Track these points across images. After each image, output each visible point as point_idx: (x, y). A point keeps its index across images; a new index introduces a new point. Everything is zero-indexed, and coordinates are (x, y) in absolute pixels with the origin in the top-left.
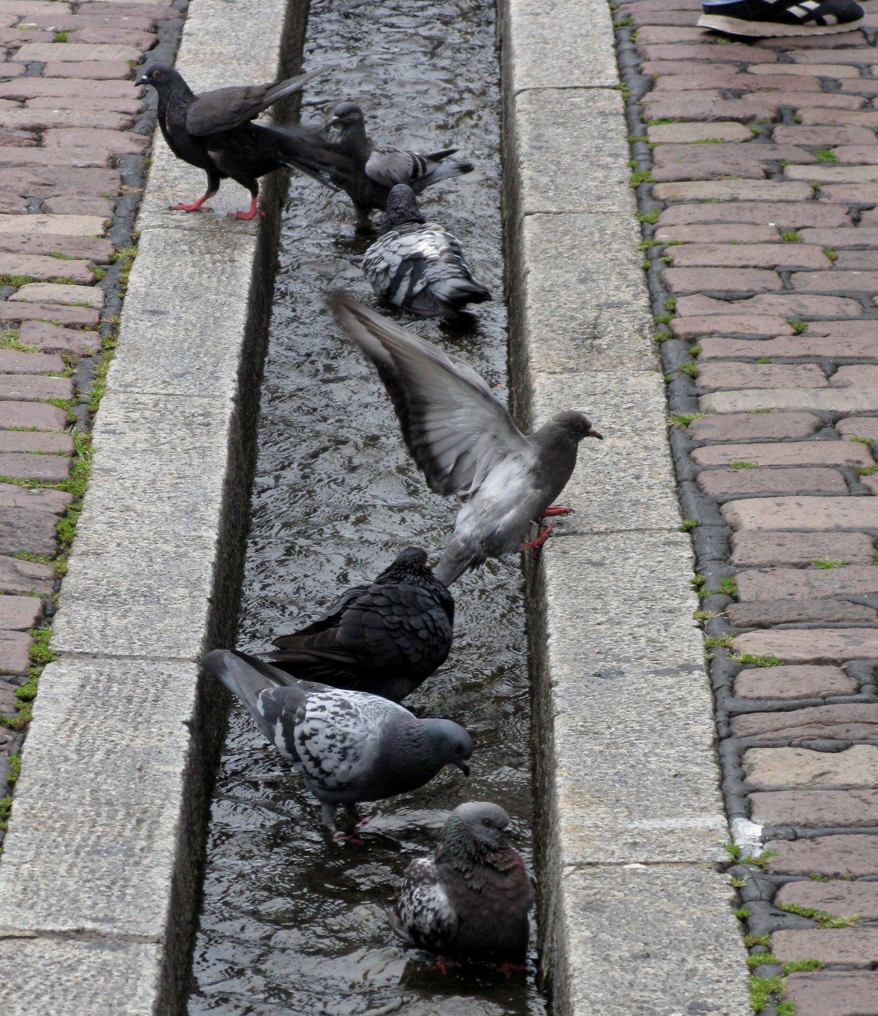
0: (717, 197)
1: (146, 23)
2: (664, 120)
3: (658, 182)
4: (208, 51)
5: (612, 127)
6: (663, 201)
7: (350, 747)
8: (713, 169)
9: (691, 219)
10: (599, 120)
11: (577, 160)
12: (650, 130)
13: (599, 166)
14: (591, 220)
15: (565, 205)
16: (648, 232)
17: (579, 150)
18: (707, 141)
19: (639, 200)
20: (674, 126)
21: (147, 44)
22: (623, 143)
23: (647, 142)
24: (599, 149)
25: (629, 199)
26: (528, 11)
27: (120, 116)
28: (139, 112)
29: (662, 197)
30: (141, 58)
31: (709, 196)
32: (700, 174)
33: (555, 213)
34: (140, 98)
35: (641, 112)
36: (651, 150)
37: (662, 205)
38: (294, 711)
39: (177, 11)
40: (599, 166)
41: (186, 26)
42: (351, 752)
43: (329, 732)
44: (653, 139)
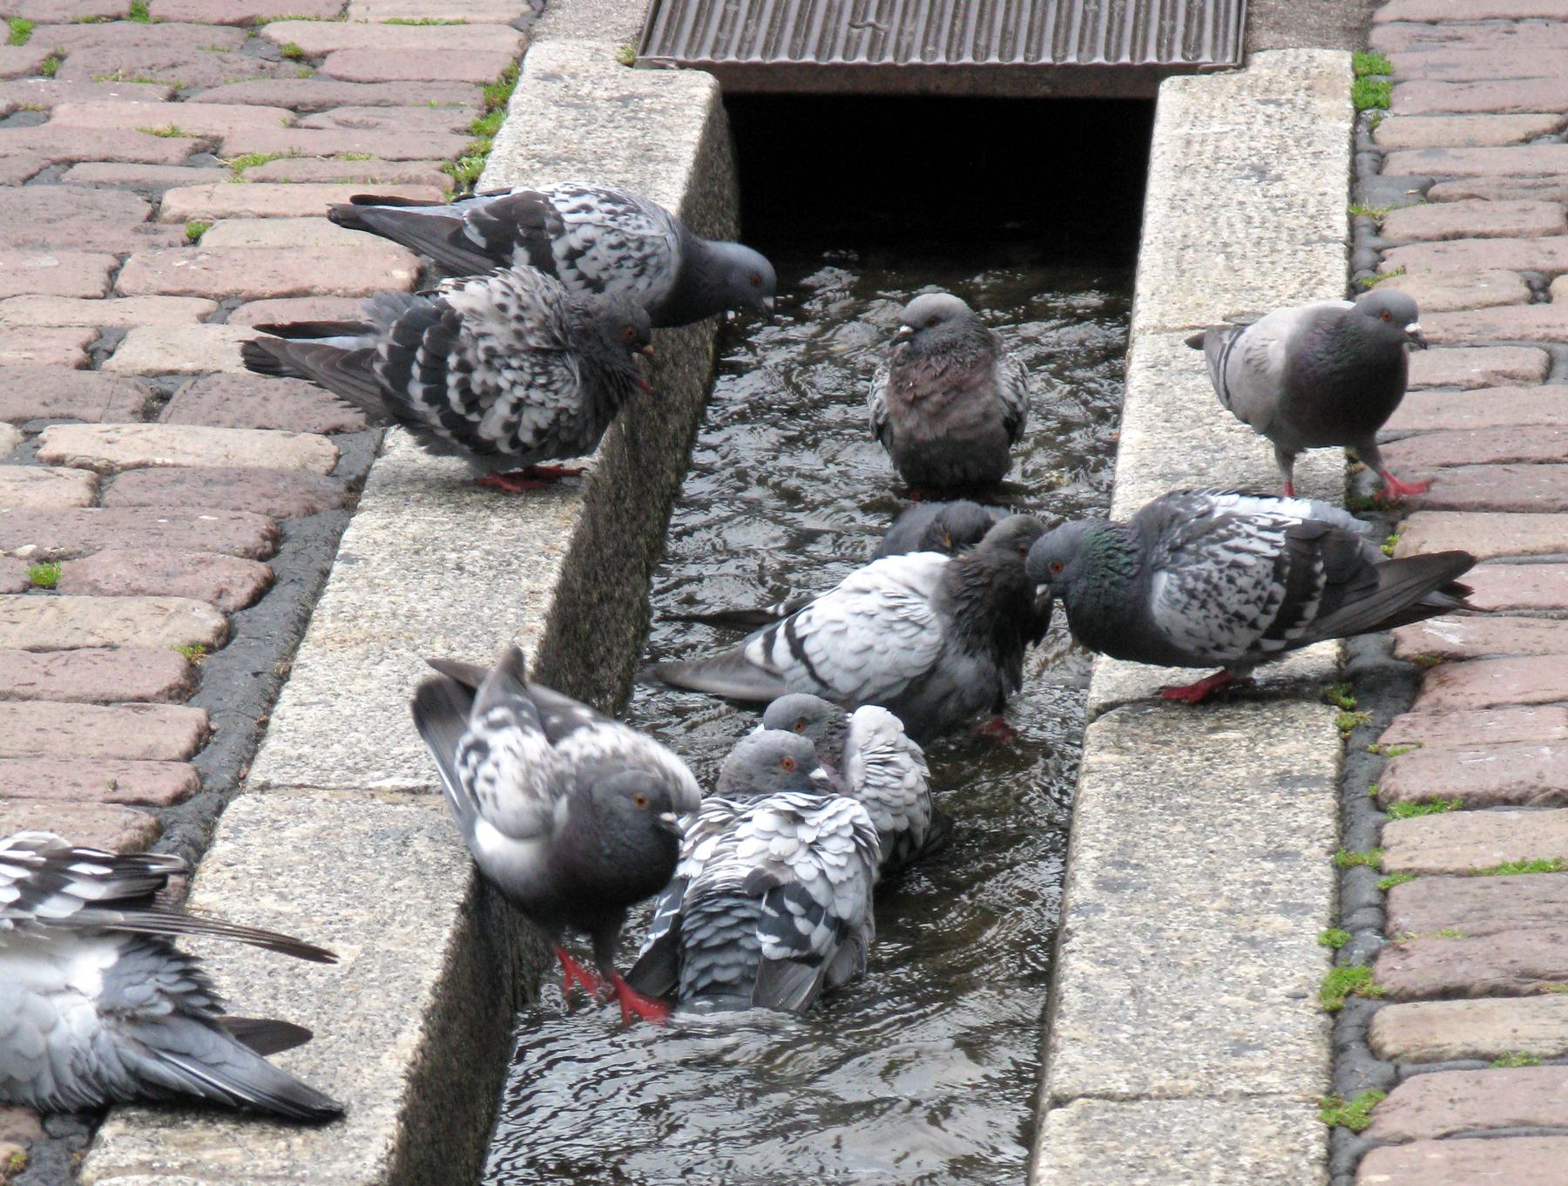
0: (1526, 1048)
1: (251, 532)
2: (1426, 803)
3: (1386, 997)
4: (385, 608)
5: (1302, 820)
6: (1391, 1058)
7: (653, 254)
8: (1526, 962)
9: (1453, 1120)
10: (1274, 798)
11: (1204, 924)
12: (1391, 831)
13: (1252, 943)
14: (1212, 1119)
15: (1153, 1073)
16: (1343, 1161)
17: (1215, 893)
18: (1521, 867)
19: (1338, 1050)
20: (1448, 821)
21: (240, 594)
22: (1323, 873)
23: (1379, 870)
24: (1263, 890)
25: (1311, 1051)
26: (1157, 469)
27: (126, 815)
28: (178, 799)
29: (1390, 1049)
30: (219, 633)
31: (1506, 1045)
32: (1492, 977)
33: (1126, 1099)
34: (188, 757)
35: (1375, 778)
36: (1385, 893)
37: (1387, 1069)
38: (541, 227)
39: (341, 488)
40: (1252, 943)
41: (349, 535)
42: (652, 261)
43: (613, 239)
44: (1392, 861)
